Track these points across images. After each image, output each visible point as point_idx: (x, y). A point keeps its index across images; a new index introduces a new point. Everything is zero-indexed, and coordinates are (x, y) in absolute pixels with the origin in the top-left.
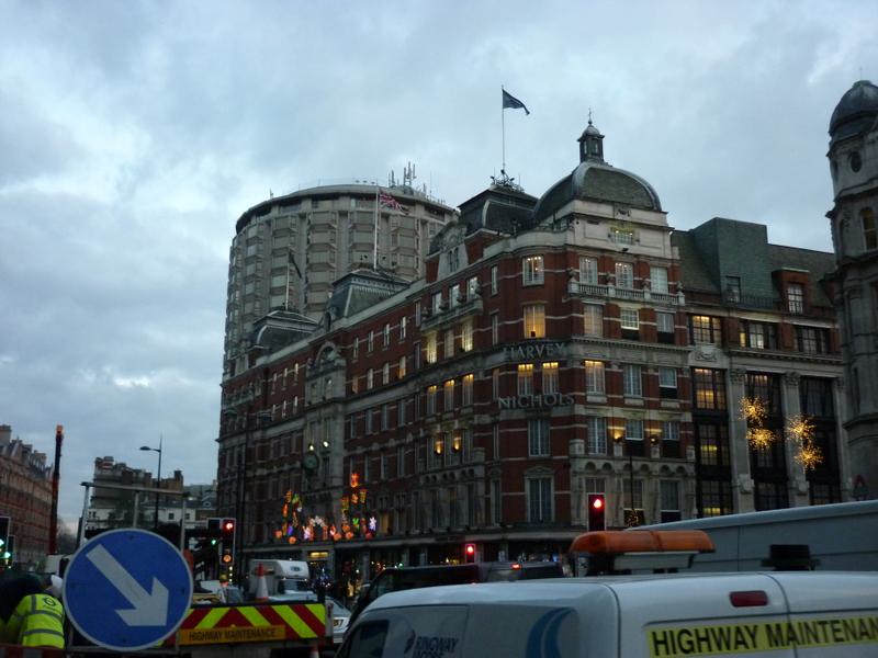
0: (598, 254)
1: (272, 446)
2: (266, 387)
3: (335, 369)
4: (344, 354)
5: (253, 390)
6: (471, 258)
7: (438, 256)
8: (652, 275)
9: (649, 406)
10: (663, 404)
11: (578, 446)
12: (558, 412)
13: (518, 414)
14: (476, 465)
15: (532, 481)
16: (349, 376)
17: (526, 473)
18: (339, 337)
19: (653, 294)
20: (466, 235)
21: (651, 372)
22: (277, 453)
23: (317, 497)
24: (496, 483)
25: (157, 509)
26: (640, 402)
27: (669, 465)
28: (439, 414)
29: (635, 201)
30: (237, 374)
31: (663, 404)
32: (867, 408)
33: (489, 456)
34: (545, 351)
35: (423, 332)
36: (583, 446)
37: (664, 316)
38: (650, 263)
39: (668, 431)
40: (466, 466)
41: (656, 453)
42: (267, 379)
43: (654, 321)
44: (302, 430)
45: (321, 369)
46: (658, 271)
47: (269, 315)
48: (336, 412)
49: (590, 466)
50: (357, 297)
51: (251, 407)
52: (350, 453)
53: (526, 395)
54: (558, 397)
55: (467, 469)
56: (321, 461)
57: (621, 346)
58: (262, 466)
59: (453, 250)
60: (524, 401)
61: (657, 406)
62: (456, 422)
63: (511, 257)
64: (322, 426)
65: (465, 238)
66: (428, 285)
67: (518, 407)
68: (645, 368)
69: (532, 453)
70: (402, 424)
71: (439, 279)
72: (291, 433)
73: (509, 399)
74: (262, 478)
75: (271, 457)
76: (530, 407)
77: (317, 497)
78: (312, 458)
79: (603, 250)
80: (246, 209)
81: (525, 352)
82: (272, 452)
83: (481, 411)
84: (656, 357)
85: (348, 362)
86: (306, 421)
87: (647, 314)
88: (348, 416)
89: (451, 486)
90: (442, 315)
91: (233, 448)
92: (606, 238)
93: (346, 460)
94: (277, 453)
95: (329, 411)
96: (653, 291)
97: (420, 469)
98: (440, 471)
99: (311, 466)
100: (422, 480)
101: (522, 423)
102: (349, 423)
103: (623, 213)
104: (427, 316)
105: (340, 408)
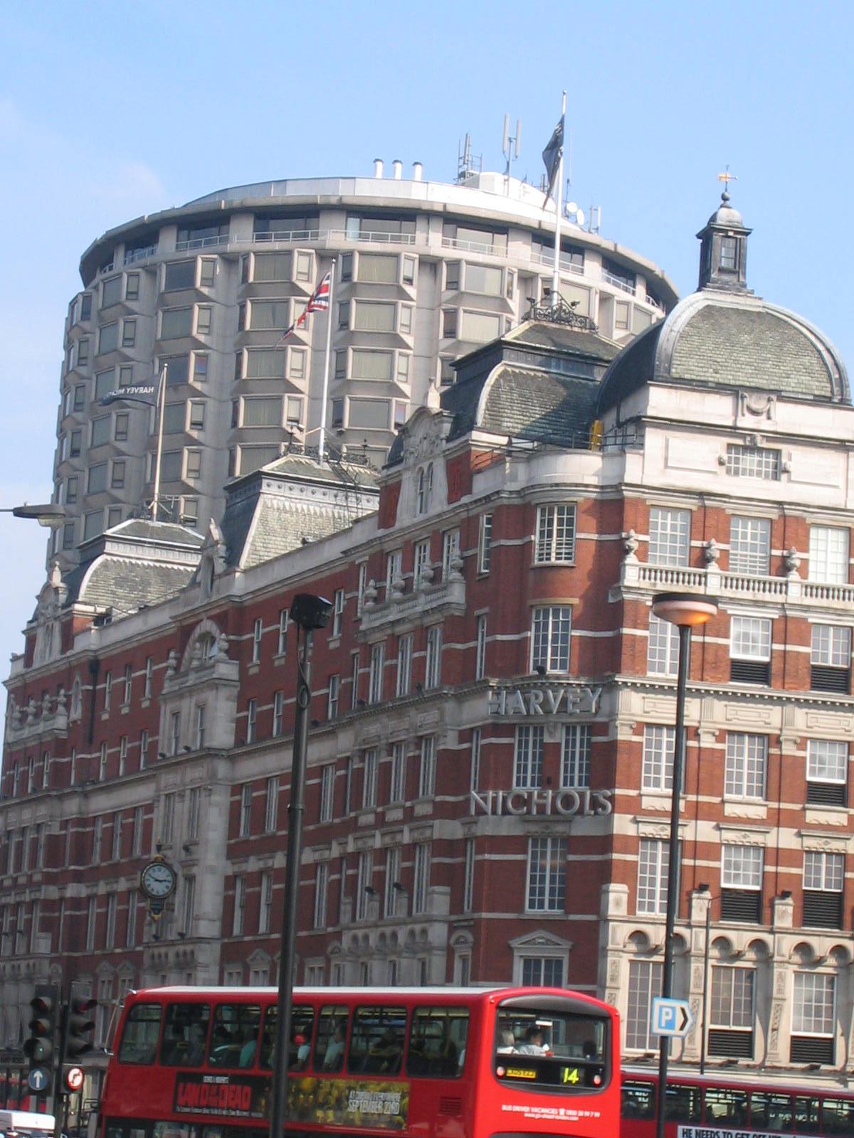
0: (692, 504)
1: (99, 835)
2: (93, 701)
3: (216, 684)
4: (237, 652)
5: (67, 706)
6: (453, 496)
7: (399, 473)
8: (812, 545)
9: (777, 819)
10: (811, 817)
11: (617, 894)
12: (582, 828)
13: (508, 827)
14: (430, 920)
15: (527, 962)
16: (243, 703)
17: (515, 943)
18: (225, 613)
19: (811, 589)
20: (449, 440)
21: (788, 750)
22: (108, 853)
23: (172, 958)
24: (464, 959)
25: (428, 233)
26: (761, 813)
27: (813, 941)
28: (408, 804)
29: (791, 385)
30: (36, 665)
31: (811, 817)
32: (2, 964)
33: (456, 906)
34: (564, 702)
35: (365, 633)
36: (625, 897)
37: (831, 629)
38: (810, 519)
39: (818, 870)
40: (416, 921)
41: (785, 912)
42: (95, 684)
43: (807, 645)
44: (149, 809)
45: (192, 679)
46: (832, 534)
47: (109, 532)
48: (213, 775)
49: (639, 937)
50: (274, 524)
51: (61, 746)
52: (236, 868)
53: (523, 791)
54: (582, 795)
55: (418, 927)
56: (181, 881)
57: (725, 696)
58: (78, 877)
59: (425, 466)
60: (520, 801)
61: (796, 821)
62: (378, 834)
63: (517, 501)
64: (187, 803)
65: (444, 445)
66: (381, 532)
67: (506, 812)
68: (776, 741)
69: (532, 906)
70: (327, 818)
71: (398, 525)
72: (133, 812)
73: (491, 794)
74: (77, 903)
75: (96, 860)
76: (529, 812)
77: (172, 958)
78: (162, 874)
79: (702, 495)
80: (98, 233)
81: (527, 702)
82: (98, 847)
83: (443, 811)
84: (801, 718)
85: (243, 671)
86: (158, 790)
87: (785, 628)
88: (237, 789)
89: (393, 958)
90: (399, 602)
91: (23, 831)
92: (715, 467)
93: (230, 882)
94: (108, 853)
95: (195, 774)
96: (812, 579)
97: (345, 919)
98: (376, 926)
99: (158, 889)
100: (346, 941)
101: (517, 844)
102: (239, 802)
103: (755, 413)
104: (375, 600)
105: (222, 768)
